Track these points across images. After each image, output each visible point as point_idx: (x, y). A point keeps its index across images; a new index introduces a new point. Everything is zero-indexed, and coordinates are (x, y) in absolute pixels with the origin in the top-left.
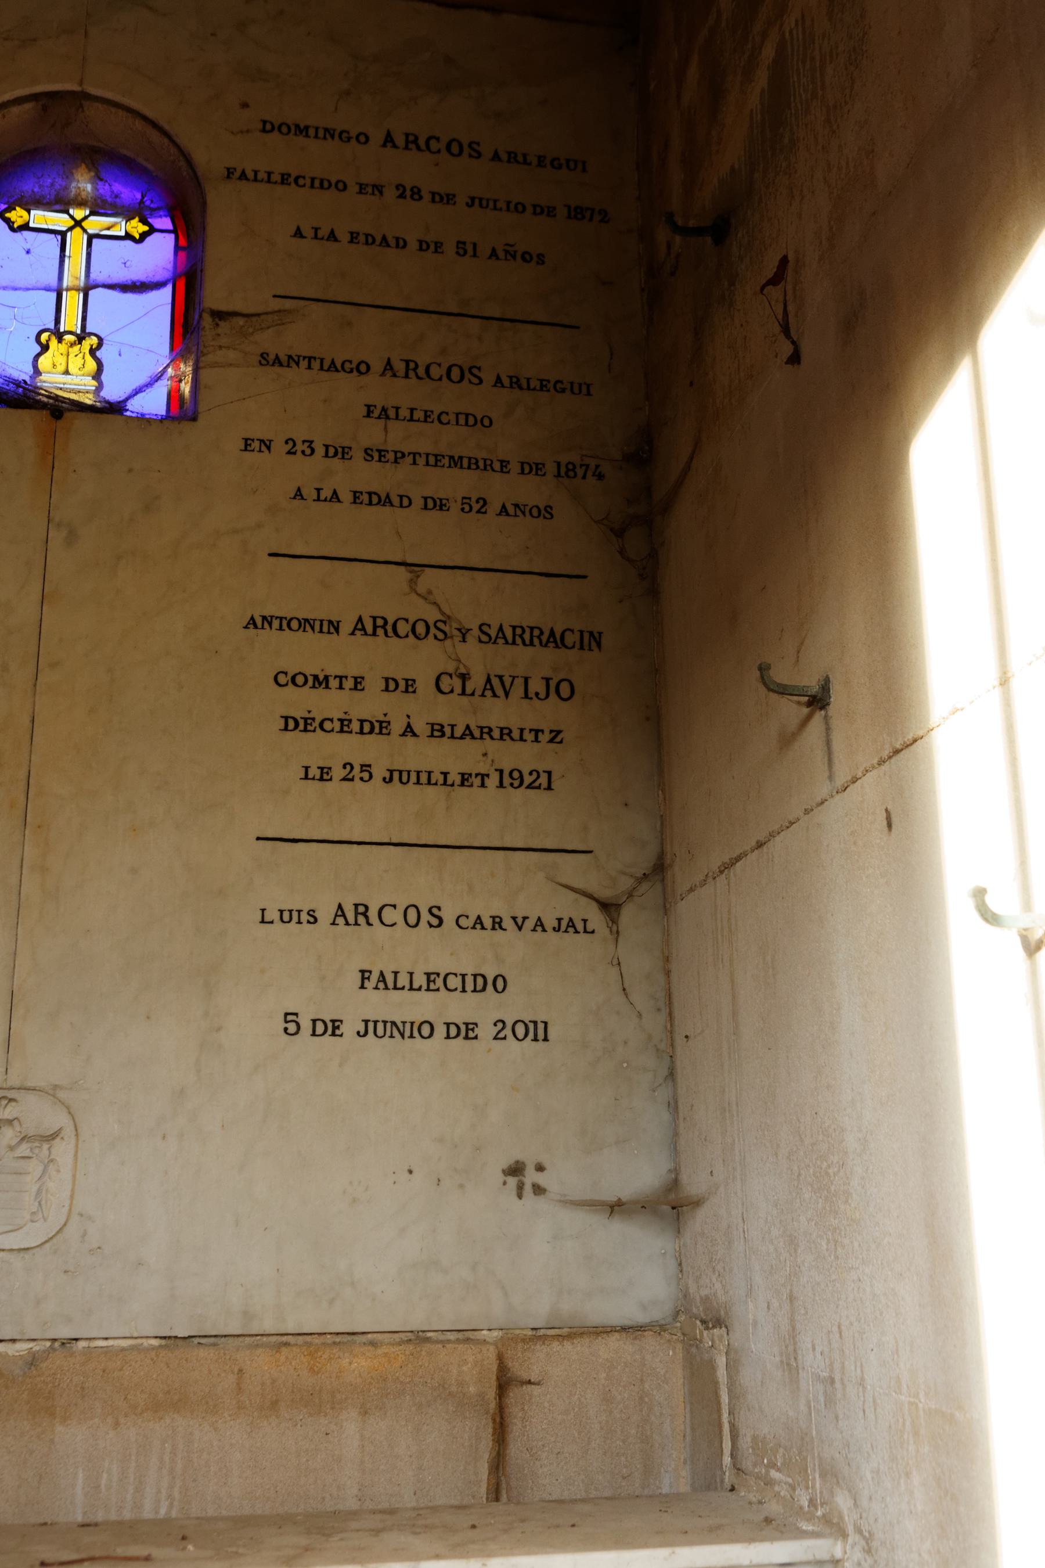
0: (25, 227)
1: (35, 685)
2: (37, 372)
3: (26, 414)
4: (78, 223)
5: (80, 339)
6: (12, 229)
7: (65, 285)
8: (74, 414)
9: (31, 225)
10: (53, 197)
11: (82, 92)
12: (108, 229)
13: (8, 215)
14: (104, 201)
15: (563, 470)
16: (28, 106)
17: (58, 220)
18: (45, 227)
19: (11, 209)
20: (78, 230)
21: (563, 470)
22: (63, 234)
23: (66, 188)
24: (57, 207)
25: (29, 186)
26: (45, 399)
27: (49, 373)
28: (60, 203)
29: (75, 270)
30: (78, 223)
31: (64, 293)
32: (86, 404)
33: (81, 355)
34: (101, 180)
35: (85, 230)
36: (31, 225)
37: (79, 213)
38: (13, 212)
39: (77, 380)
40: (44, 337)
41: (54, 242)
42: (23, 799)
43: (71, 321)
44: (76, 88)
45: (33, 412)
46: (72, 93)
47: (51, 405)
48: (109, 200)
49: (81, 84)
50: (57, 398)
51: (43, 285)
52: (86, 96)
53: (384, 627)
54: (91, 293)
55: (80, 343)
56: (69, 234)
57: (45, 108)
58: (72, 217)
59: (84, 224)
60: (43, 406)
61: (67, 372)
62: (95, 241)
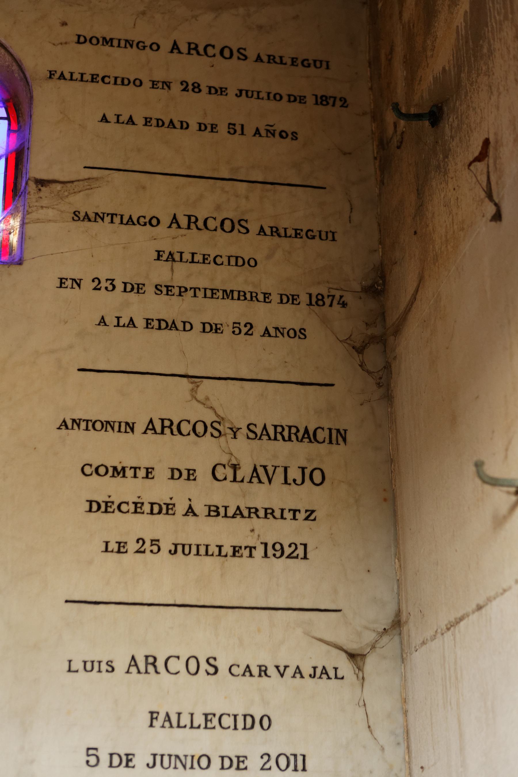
15: (314, 300)
21: (314, 300)
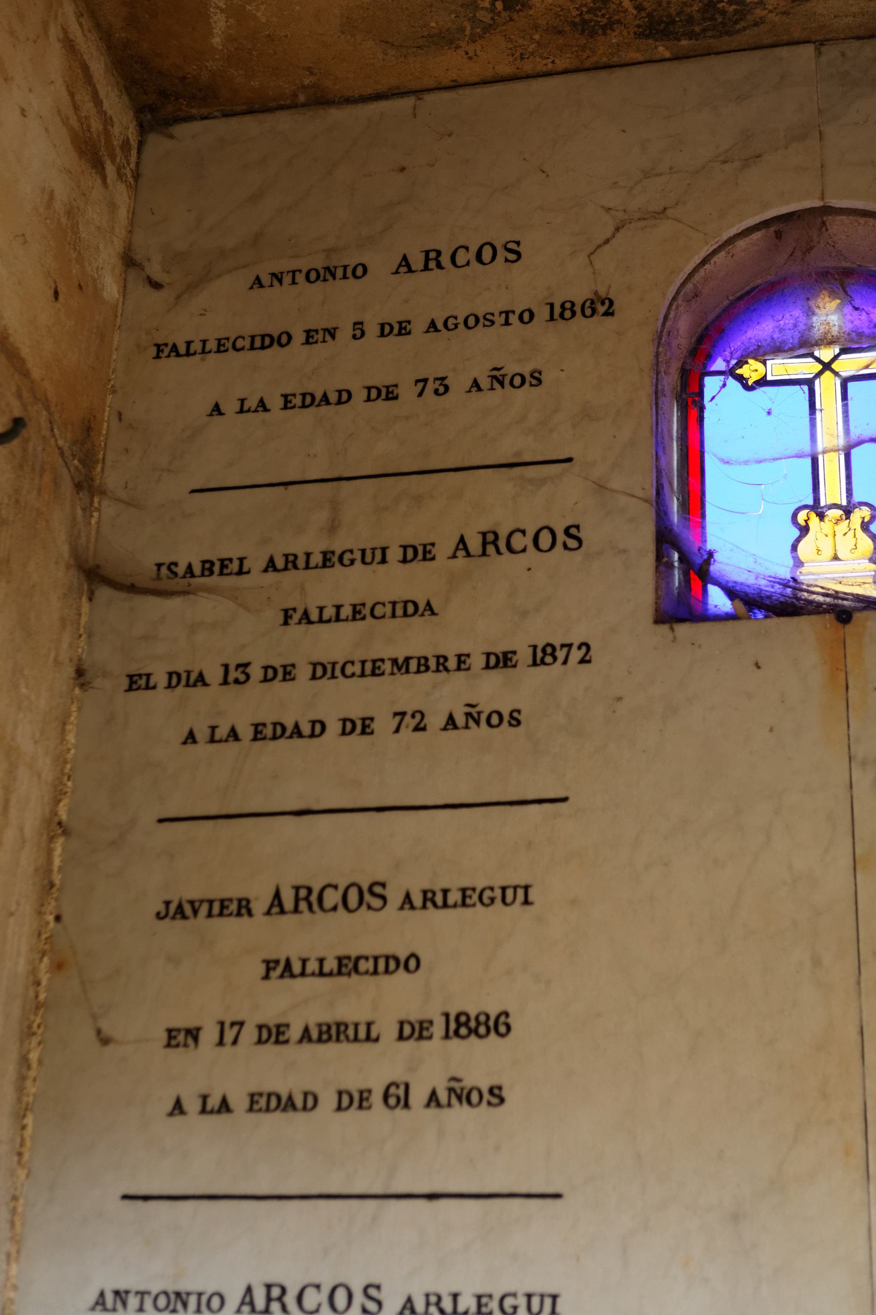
0: (763, 382)
1: (859, 983)
2: (798, 563)
3: (803, 622)
4: (827, 366)
5: (848, 512)
6: (748, 388)
7: (820, 448)
8: (865, 613)
9: (769, 378)
10: (796, 341)
11: (824, 206)
12: (867, 367)
13: (739, 371)
14: (860, 335)
16: (756, 236)
17: (805, 368)
18: (787, 377)
19: (741, 363)
20: (828, 374)
22: (809, 383)
23: (810, 327)
24: (802, 351)
25: (764, 329)
26: (821, 599)
27: (813, 561)
28: (804, 346)
29: (830, 429)
30: (827, 366)
31: (820, 458)
32: (669, 519)
33: (852, 532)
34: (856, 309)
35: (836, 374)
36: (769, 378)
37: (826, 354)
38: (745, 367)
39: (850, 567)
40: (802, 517)
41: (800, 394)
42: (860, 1141)
43: (833, 491)
44: (817, 203)
45: (814, 618)
46: (811, 211)
47: (829, 605)
48: (867, 331)
49: (822, 198)
50: (836, 595)
51: (794, 453)
52: (828, 210)
53: (495, 543)
54: (854, 452)
55: (848, 518)
56: (817, 382)
57: (779, 235)
58: (818, 360)
59: (834, 366)
60: (816, 609)
61: (836, 558)
62: (850, 385)
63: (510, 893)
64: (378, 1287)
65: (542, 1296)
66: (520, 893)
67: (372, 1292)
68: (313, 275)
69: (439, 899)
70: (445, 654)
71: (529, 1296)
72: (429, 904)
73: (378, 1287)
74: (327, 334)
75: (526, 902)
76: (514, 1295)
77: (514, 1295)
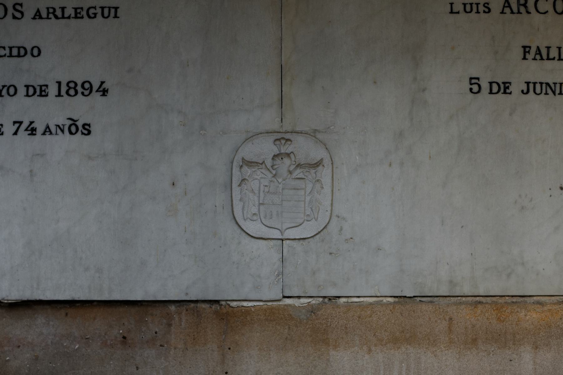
63: (106, 11)
64: (21, 5)
65: (109, 8)
66: (113, 11)
67: (18, 7)
68: (12, 91)
69: (59, 13)
70: (72, 136)
71: (103, 8)
72: (51, 16)
73: (21, 5)
74: (58, 128)
75: (116, 16)
76: (95, 8)
77: (95, 8)
